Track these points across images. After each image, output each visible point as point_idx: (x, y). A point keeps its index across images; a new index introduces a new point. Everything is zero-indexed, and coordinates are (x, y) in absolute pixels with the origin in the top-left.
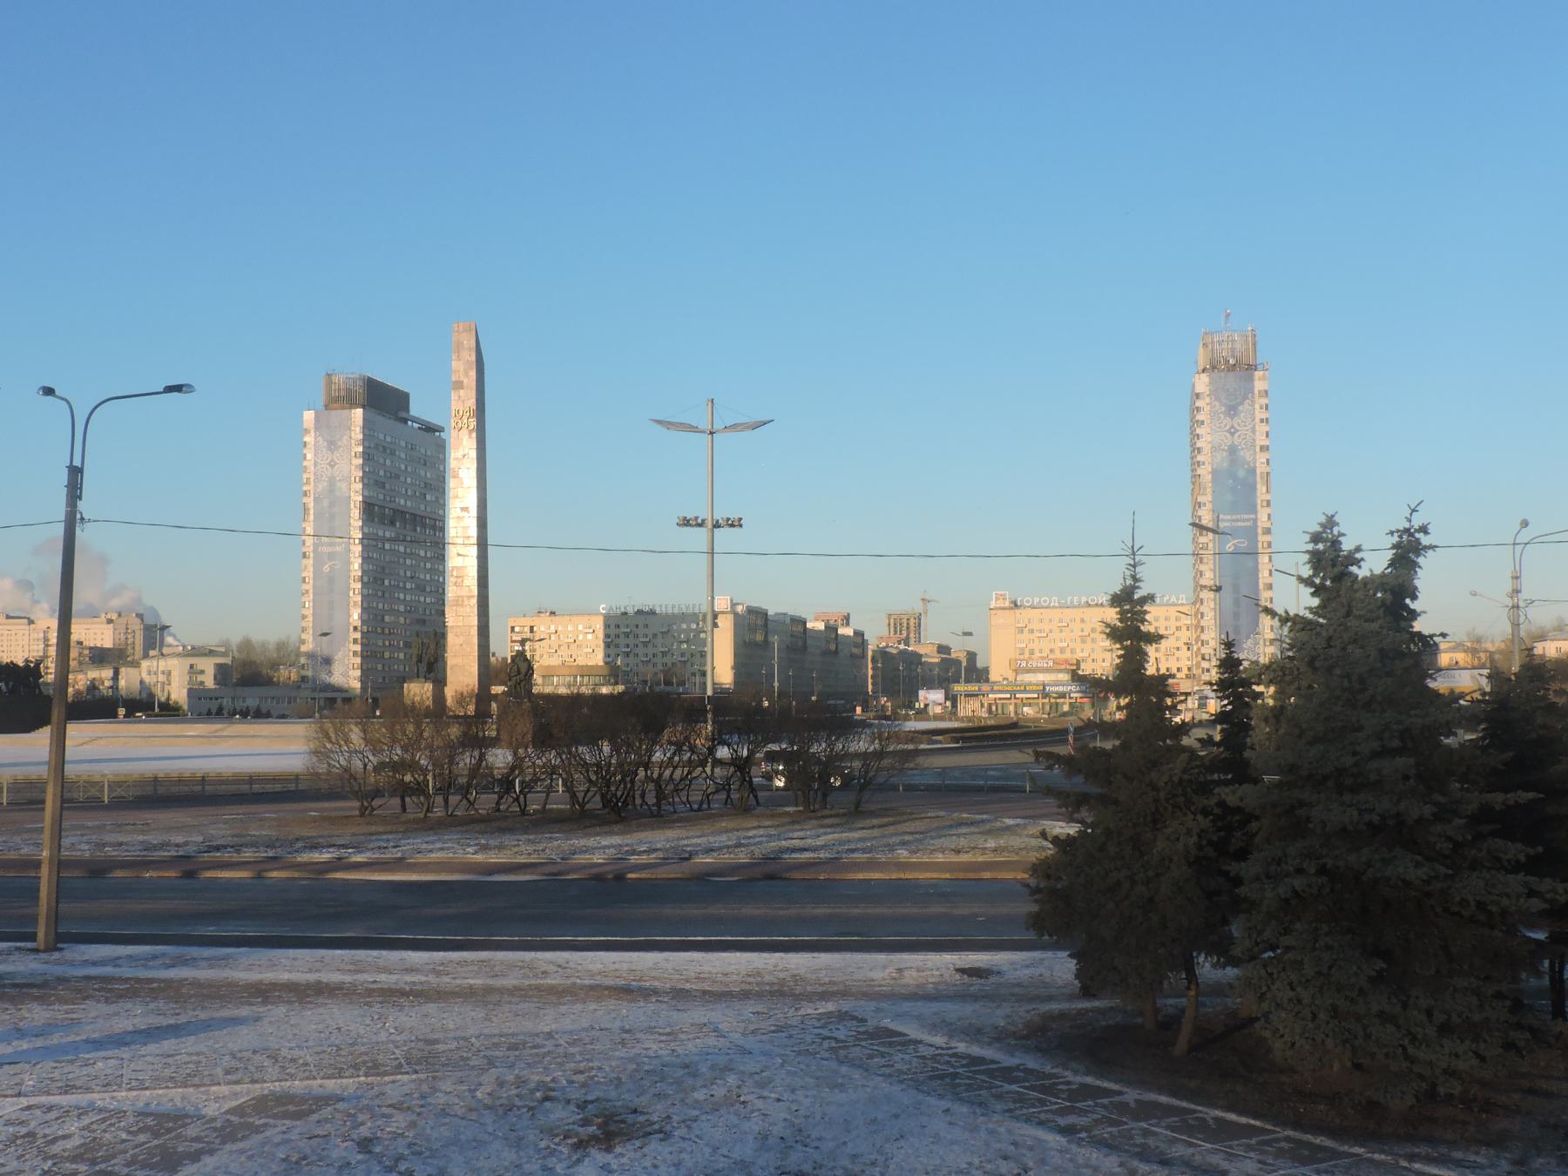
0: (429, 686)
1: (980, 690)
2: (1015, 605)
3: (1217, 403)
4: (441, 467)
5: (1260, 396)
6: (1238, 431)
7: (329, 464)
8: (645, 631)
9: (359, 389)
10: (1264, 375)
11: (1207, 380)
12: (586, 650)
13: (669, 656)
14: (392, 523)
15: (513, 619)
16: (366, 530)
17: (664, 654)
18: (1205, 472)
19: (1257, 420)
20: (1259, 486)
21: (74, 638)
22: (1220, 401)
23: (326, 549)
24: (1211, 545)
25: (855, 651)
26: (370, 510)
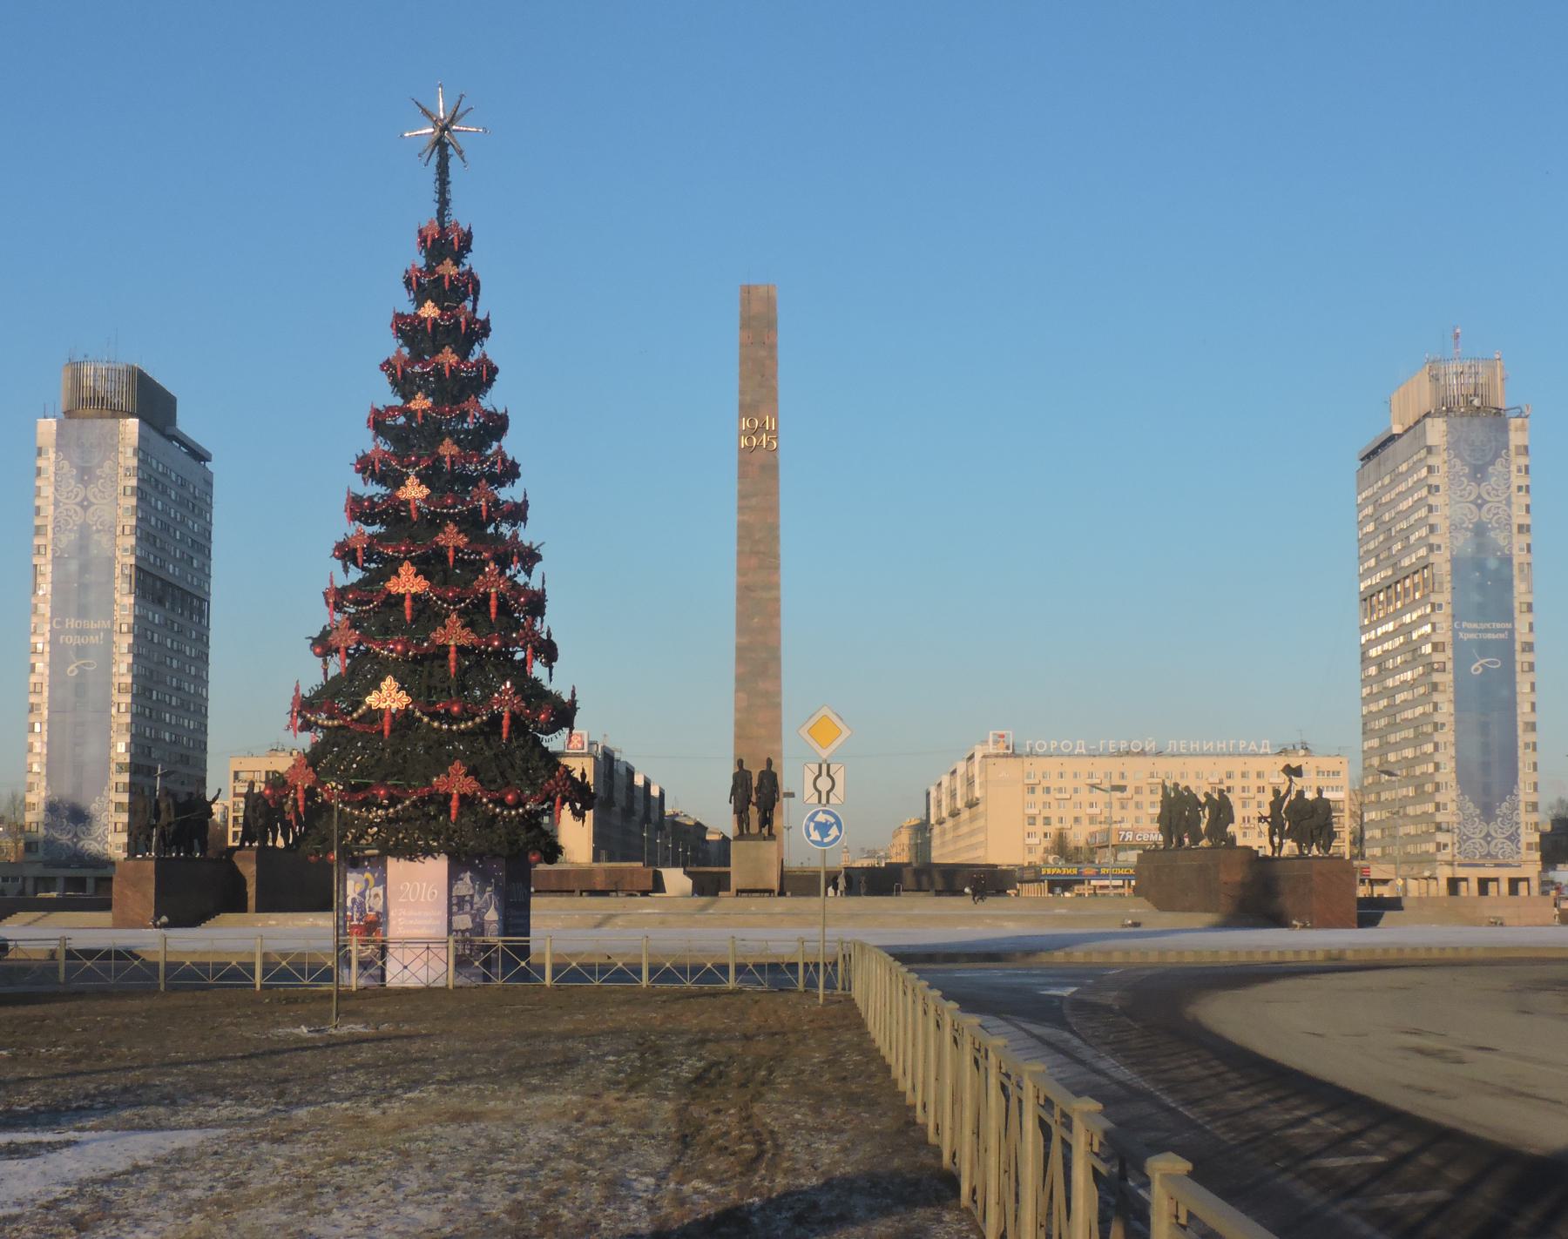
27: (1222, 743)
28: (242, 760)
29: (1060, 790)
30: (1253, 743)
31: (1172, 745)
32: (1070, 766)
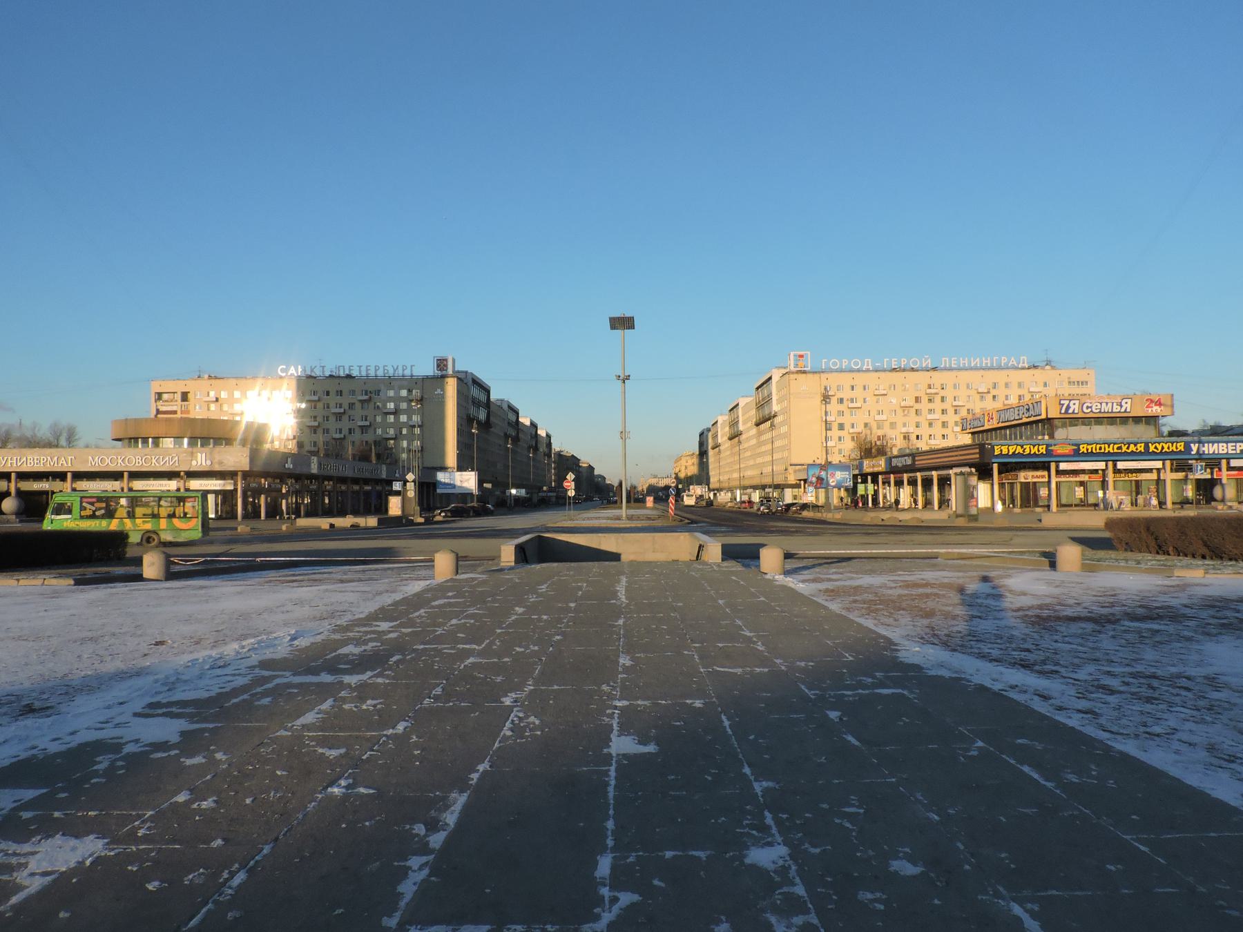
0: (880, 476)
13: (371, 431)
17: (363, 429)
21: (1047, 489)
27: (964, 360)
28: (162, 383)
29: (852, 400)
30: (1013, 359)
31: (945, 361)
32: (860, 379)
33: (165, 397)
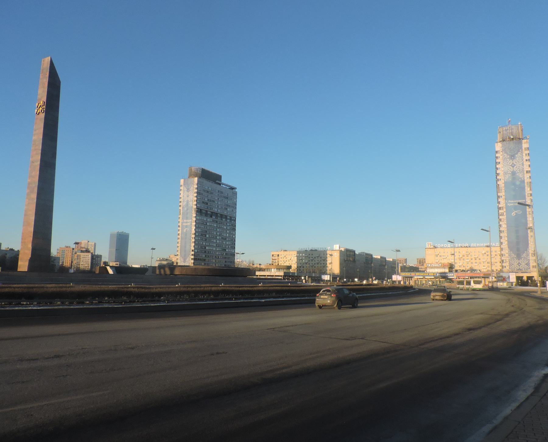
1: (410, 275)
2: (435, 247)
3: (506, 155)
4: (235, 201)
5: (525, 150)
6: (517, 264)
7: (187, 196)
8: (312, 256)
9: (199, 172)
10: (527, 141)
11: (501, 145)
12: (294, 262)
14: (211, 217)
15: (272, 252)
16: (198, 218)
18: (501, 183)
19: (524, 160)
20: (526, 188)
22: (507, 154)
23: (185, 224)
24: (505, 214)
25: (393, 265)
26: (199, 211)
31: (472, 245)
33: (274, 255)
